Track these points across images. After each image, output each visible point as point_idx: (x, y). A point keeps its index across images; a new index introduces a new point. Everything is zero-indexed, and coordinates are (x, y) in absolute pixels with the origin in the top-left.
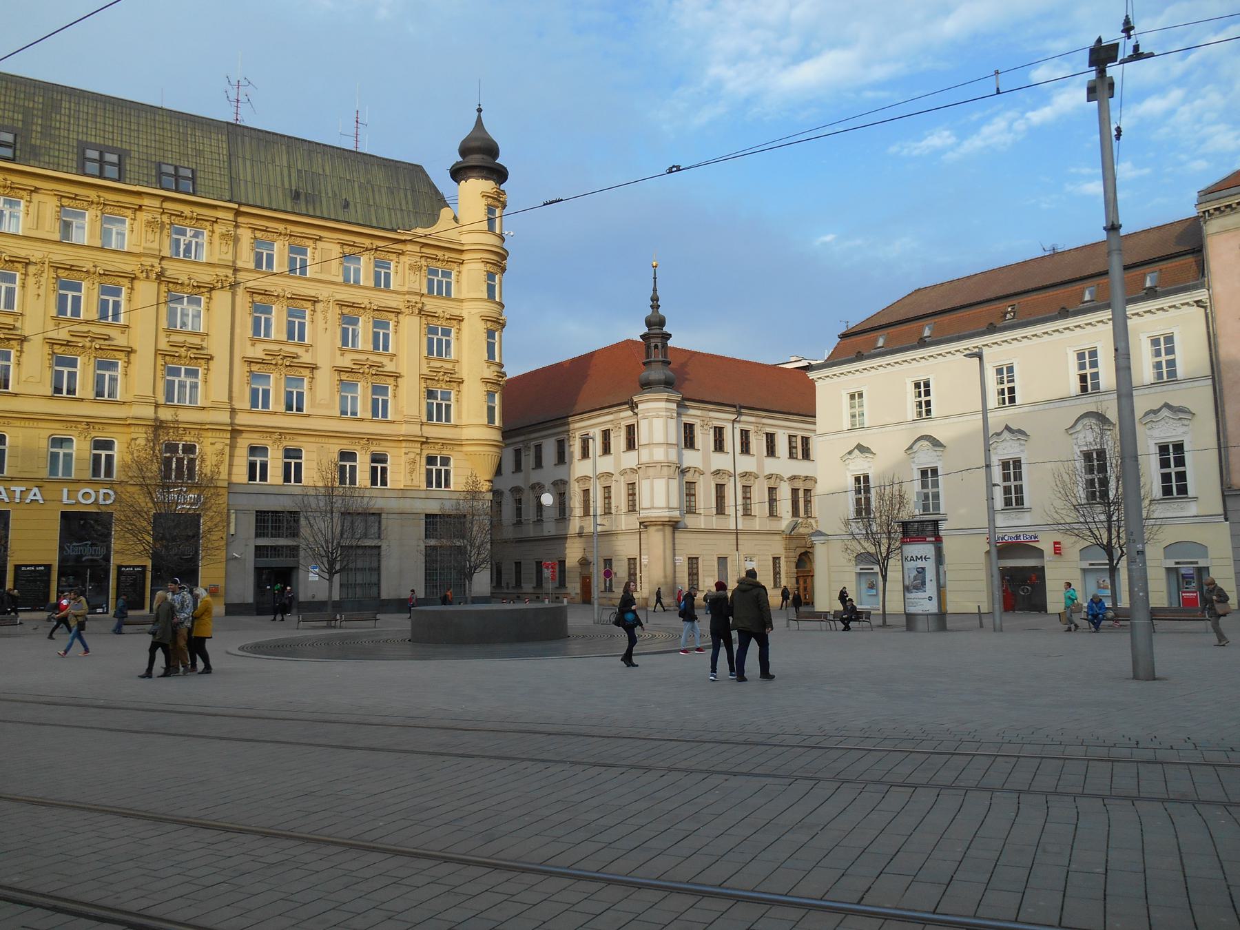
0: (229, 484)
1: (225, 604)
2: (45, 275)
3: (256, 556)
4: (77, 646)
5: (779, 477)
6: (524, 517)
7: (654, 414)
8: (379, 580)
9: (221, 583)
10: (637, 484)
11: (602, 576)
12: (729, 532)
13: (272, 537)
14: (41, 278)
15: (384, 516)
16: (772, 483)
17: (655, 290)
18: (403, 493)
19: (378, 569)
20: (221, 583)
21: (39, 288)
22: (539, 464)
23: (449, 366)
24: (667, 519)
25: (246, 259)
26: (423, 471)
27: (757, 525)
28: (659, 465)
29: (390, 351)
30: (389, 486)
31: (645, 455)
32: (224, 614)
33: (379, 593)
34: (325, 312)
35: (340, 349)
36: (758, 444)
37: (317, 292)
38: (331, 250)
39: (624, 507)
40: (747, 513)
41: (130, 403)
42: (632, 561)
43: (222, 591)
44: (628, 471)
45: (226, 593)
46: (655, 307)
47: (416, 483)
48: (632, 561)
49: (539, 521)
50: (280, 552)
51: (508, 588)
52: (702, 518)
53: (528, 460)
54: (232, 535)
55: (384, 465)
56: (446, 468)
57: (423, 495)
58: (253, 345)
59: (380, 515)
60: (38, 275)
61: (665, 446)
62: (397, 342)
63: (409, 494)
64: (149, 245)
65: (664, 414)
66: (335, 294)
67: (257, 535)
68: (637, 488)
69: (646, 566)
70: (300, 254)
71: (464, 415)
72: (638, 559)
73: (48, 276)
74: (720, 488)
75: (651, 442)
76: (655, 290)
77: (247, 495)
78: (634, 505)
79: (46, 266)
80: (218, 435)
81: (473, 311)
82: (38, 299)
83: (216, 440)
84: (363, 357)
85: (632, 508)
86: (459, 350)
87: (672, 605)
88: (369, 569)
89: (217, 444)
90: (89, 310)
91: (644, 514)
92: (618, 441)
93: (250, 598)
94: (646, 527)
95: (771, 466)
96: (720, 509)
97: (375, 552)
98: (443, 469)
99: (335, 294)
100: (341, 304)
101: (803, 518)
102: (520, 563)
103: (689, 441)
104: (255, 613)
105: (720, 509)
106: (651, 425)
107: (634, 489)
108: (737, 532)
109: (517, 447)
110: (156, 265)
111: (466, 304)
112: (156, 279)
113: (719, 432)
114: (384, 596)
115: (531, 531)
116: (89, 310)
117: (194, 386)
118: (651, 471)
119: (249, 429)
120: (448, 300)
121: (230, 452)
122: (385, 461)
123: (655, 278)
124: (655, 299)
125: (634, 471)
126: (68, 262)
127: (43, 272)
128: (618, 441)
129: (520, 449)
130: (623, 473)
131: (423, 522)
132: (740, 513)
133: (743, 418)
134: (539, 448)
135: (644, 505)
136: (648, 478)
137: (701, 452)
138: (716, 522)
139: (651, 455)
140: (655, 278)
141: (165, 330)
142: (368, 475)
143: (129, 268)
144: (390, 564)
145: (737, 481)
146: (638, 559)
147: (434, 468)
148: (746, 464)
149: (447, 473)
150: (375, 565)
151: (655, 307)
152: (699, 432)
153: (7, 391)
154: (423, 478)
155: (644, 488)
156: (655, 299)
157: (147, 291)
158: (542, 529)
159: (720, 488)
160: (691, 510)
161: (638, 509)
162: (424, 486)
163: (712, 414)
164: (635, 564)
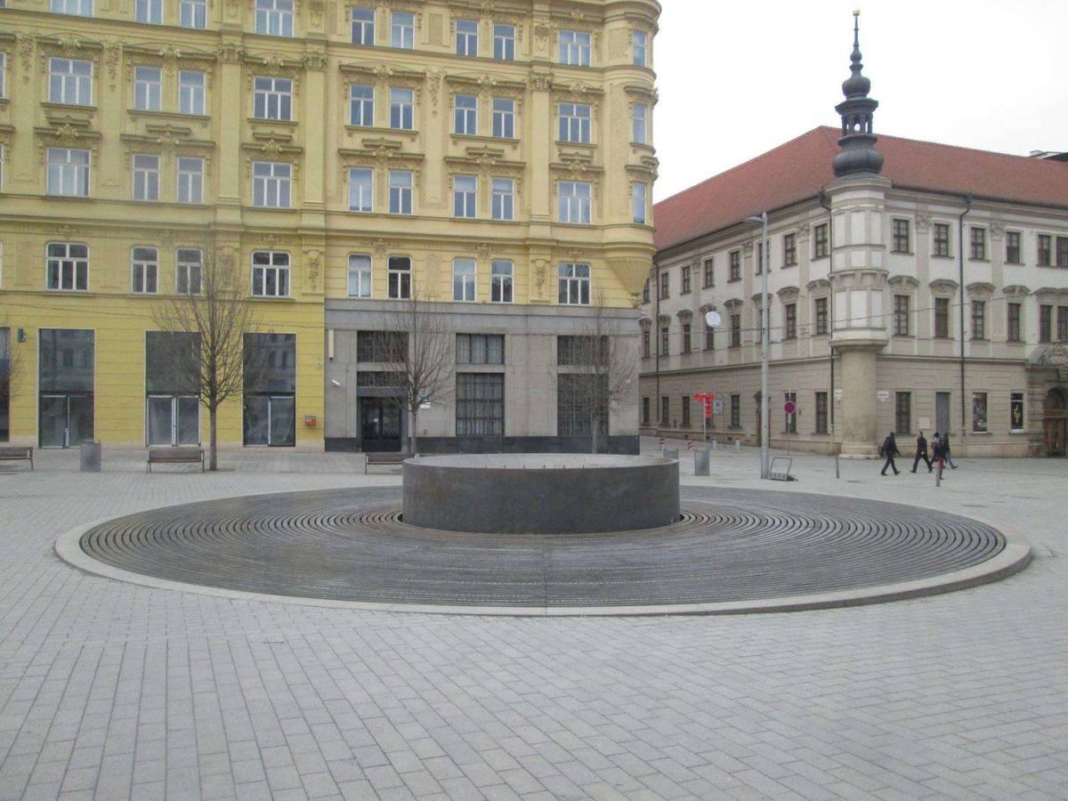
0: (326, 299)
1: (326, 439)
2: (33, 54)
3: (359, 384)
4: (890, 470)
5: (1024, 291)
6: (693, 346)
7: (853, 206)
8: (503, 414)
9: (320, 415)
10: (829, 300)
11: (783, 412)
12: (950, 361)
13: (376, 361)
14: (29, 58)
15: (507, 338)
16: (821, 293)
17: (856, 45)
18: (528, 312)
19: (502, 401)
20: (320, 415)
21: (113, 78)
22: (709, 284)
23: (587, 152)
24: (869, 343)
25: (344, 33)
26: (556, 282)
27: (990, 352)
28: (858, 275)
29: (413, 128)
30: (513, 302)
31: (840, 262)
32: (324, 450)
33: (503, 430)
34: (434, 91)
35: (348, 128)
36: (996, 248)
37: (425, 68)
38: (441, 15)
39: (811, 330)
40: (979, 336)
41: (603, 228)
42: (821, 396)
43: (321, 423)
44: (818, 285)
45: (325, 427)
46: (856, 66)
47: (545, 298)
48: (821, 396)
49: (710, 345)
50: (386, 380)
51: (675, 426)
52: (991, 346)
53: (697, 278)
54: (331, 359)
55: (585, 279)
56: (282, 267)
57: (554, 312)
58: (350, 135)
59: (502, 337)
60: (26, 54)
61: (868, 248)
62: (423, 118)
63: (536, 311)
64: (314, 30)
65: (868, 205)
66: (446, 70)
67: (359, 360)
68: (829, 306)
69: (839, 402)
70: (365, 19)
71: (606, 211)
72: (829, 394)
73: (442, 92)
74: (942, 304)
75: (849, 243)
76: (856, 45)
77: (348, 313)
78: (825, 327)
79: (120, 53)
80: (312, 242)
81: (616, 82)
82: (113, 91)
83: (310, 248)
84: (481, 145)
85: (822, 329)
86: (600, 133)
87: (873, 452)
88: (490, 401)
89: (310, 253)
90: (484, 128)
91: (837, 336)
92: (805, 247)
93: (352, 432)
94: (840, 354)
95: (1012, 275)
96: (942, 331)
97: (498, 380)
98: (580, 280)
99: (446, 70)
100: (451, 81)
101: (1054, 343)
102: (667, 398)
103: (901, 243)
104: (360, 449)
105: (942, 331)
106: (848, 225)
107: (825, 306)
108: (963, 362)
109: (735, 248)
110: (239, 43)
111: (609, 75)
112: (239, 60)
113: (942, 229)
114: (509, 433)
115: (699, 361)
116: (484, 128)
117: (285, 185)
118: (848, 282)
119: (347, 234)
120: (472, 60)
121: (325, 263)
122: (408, 267)
123: (856, 30)
124: (856, 57)
125: (824, 284)
126: (465, 76)
127: (117, 59)
128: (805, 247)
129: (738, 252)
130: (812, 286)
131: (354, 340)
132: (968, 336)
133: (972, 212)
134: (709, 262)
135: (838, 325)
136: (844, 290)
137: (914, 258)
138: (932, 348)
139: (848, 260)
140: (856, 30)
141: (558, 143)
142: (489, 289)
143: (517, 79)
144: (514, 392)
145: (965, 295)
146: (829, 394)
147: (264, 268)
148: (977, 273)
149: (283, 275)
150: (497, 396)
151: (856, 66)
152: (914, 230)
153: (497, 220)
154: (556, 291)
155: (839, 303)
156: (856, 57)
157: (540, 103)
158: (713, 358)
159: (942, 304)
160: (902, 332)
161: (829, 330)
162: (555, 301)
163: (932, 208)
164: (825, 399)
